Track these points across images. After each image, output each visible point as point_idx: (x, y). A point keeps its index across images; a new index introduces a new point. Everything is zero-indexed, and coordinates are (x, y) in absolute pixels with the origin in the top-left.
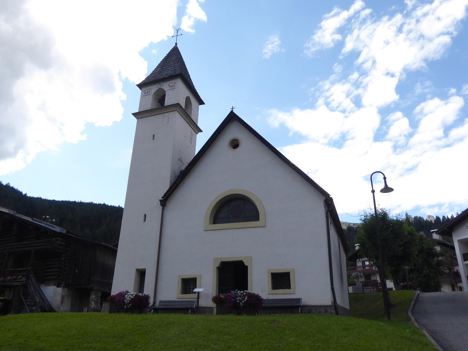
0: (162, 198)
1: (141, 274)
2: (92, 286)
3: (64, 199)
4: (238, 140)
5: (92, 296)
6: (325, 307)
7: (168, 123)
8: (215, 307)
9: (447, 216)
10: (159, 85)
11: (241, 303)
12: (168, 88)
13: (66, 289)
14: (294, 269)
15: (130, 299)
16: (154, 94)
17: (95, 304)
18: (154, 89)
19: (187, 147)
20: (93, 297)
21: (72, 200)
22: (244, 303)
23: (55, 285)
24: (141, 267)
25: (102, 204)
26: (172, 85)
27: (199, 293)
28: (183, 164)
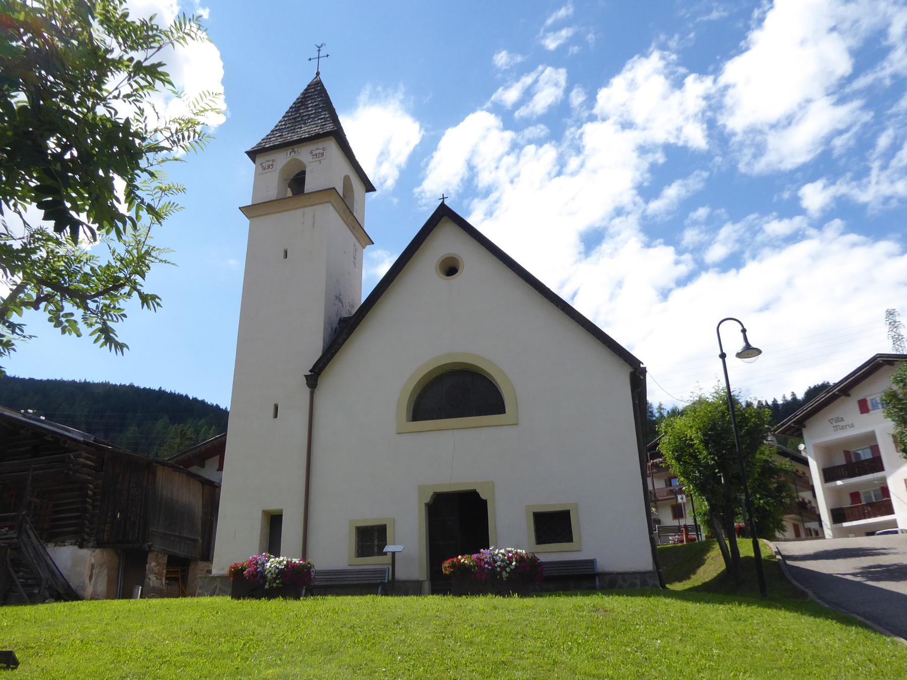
0: (311, 371)
1: (274, 521)
2: (150, 543)
3: (52, 377)
4: (457, 259)
5: (150, 564)
6: (642, 575)
7: (313, 227)
8: (426, 581)
9: (766, 401)
10: (291, 152)
11: (504, 573)
12: (310, 158)
13: (98, 551)
14: (577, 504)
15: (277, 571)
16: (282, 169)
17: (157, 579)
18: (282, 159)
19: (349, 274)
20: (152, 564)
21: (68, 377)
22: (509, 573)
23: (75, 544)
24: (273, 507)
25: (127, 385)
26: (318, 152)
27: (393, 553)
28: (343, 305)
